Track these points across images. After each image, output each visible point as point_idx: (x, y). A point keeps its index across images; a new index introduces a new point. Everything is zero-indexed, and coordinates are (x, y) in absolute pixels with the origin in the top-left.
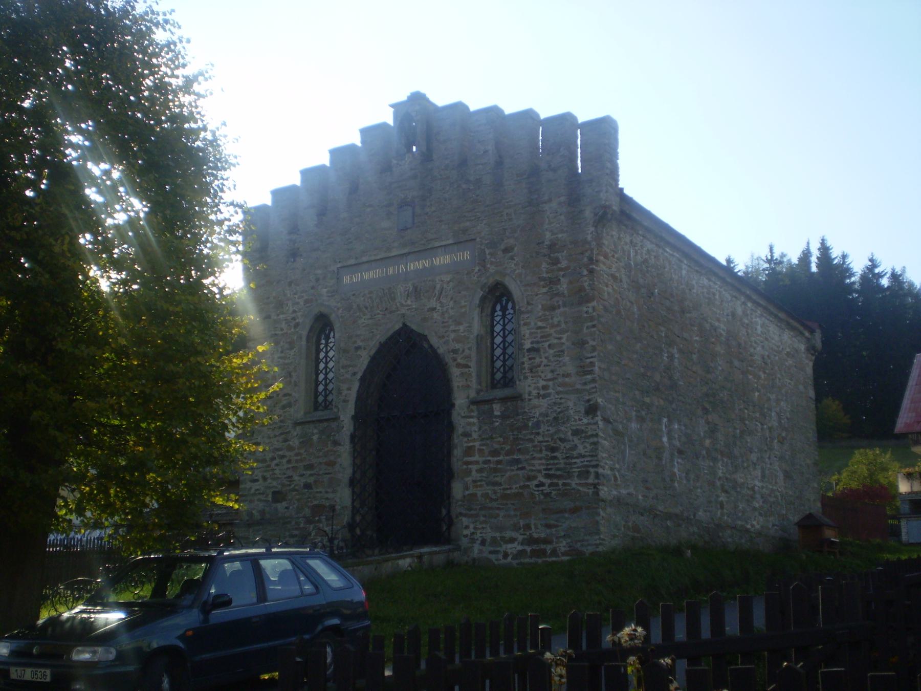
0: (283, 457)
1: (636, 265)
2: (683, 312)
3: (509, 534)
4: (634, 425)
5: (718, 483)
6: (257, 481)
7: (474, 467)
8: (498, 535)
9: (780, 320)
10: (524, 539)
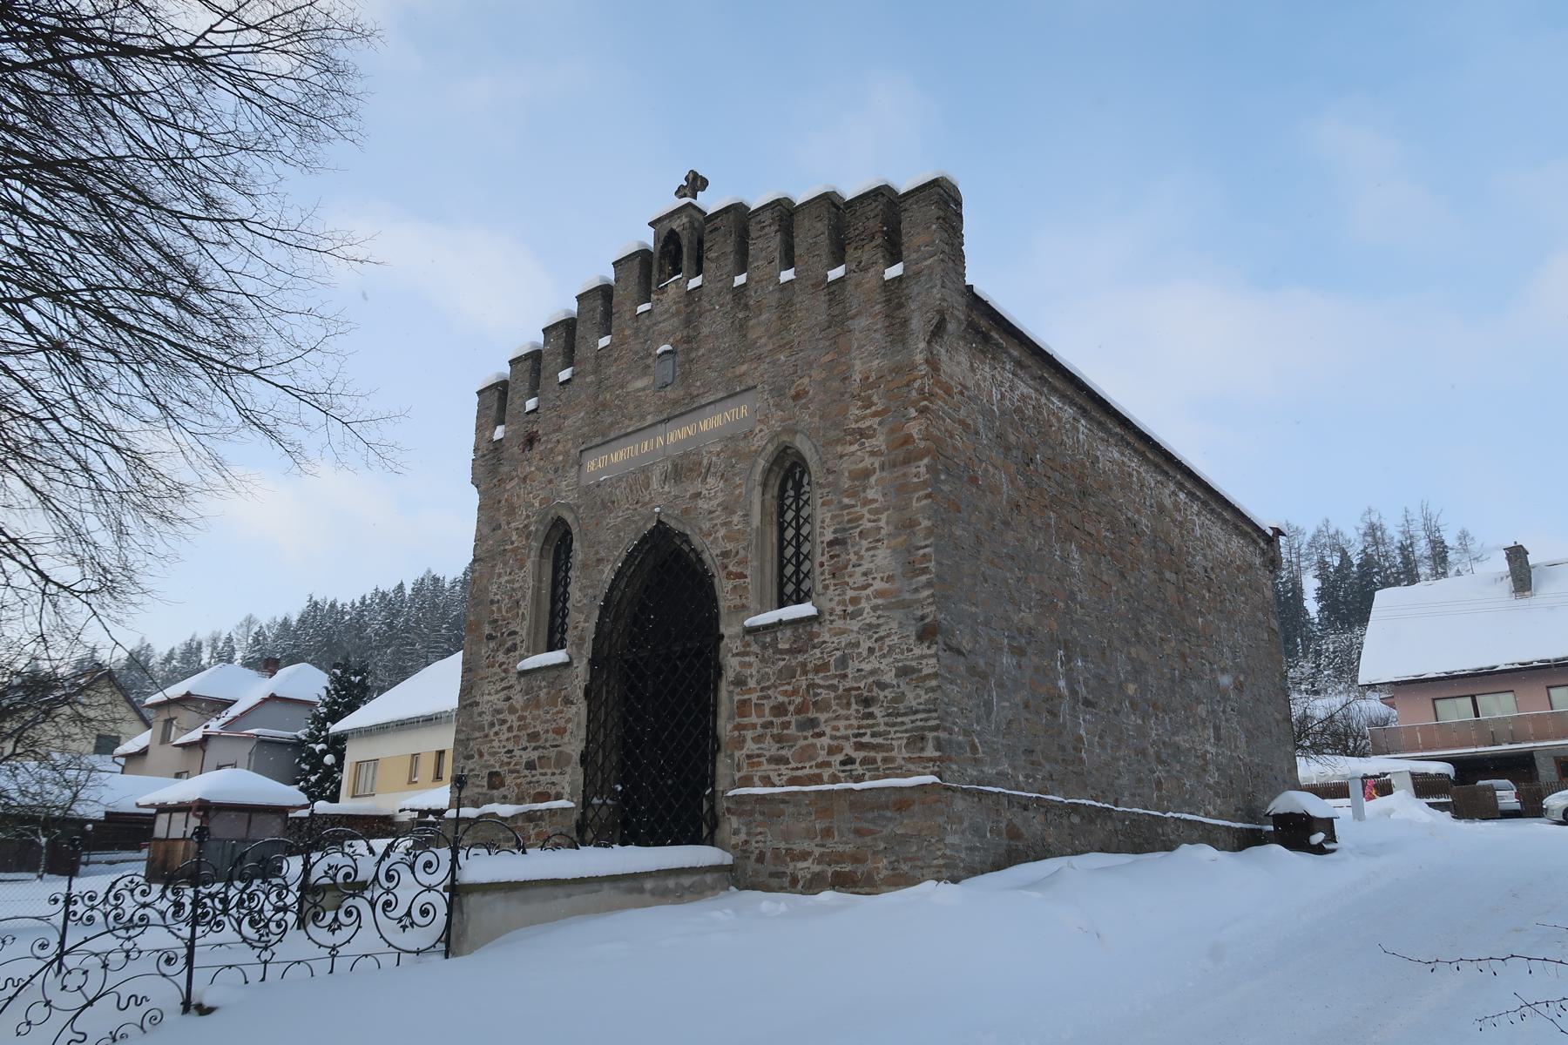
0: (504, 722)
1: (1003, 413)
2: (1084, 493)
3: (800, 845)
4: (1006, 659)
5: (1151, 751)
6: (472, 757)
7: (749, 734)
8: (782, 845)
9: (1225, 521)
10: (822, 855)
